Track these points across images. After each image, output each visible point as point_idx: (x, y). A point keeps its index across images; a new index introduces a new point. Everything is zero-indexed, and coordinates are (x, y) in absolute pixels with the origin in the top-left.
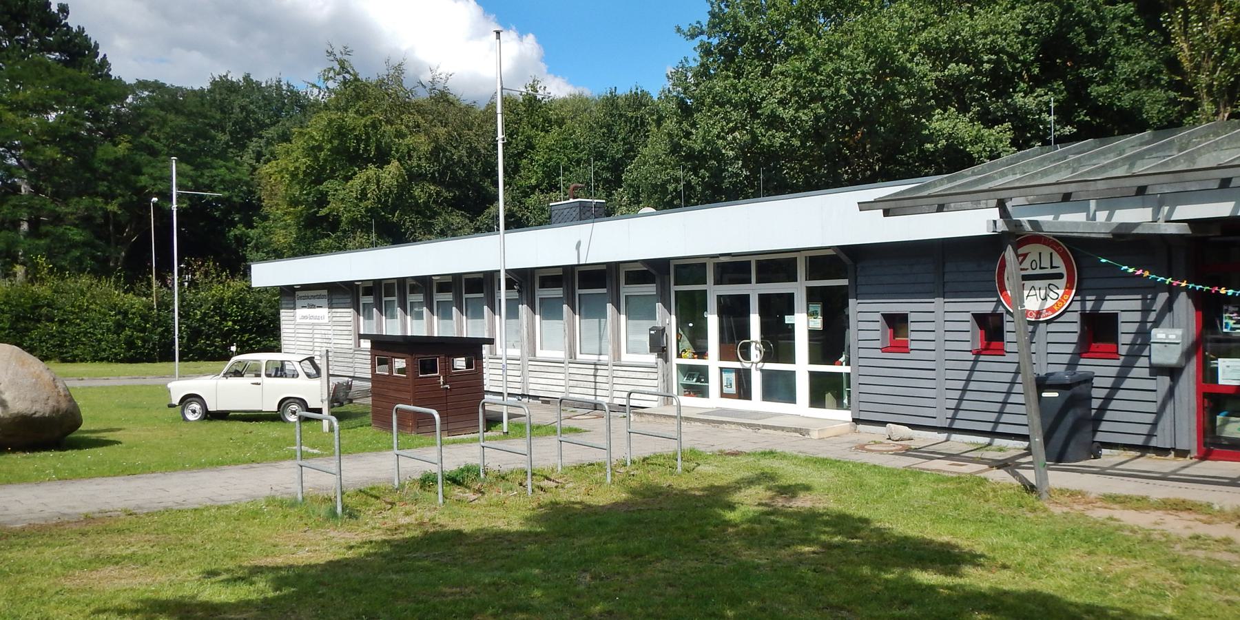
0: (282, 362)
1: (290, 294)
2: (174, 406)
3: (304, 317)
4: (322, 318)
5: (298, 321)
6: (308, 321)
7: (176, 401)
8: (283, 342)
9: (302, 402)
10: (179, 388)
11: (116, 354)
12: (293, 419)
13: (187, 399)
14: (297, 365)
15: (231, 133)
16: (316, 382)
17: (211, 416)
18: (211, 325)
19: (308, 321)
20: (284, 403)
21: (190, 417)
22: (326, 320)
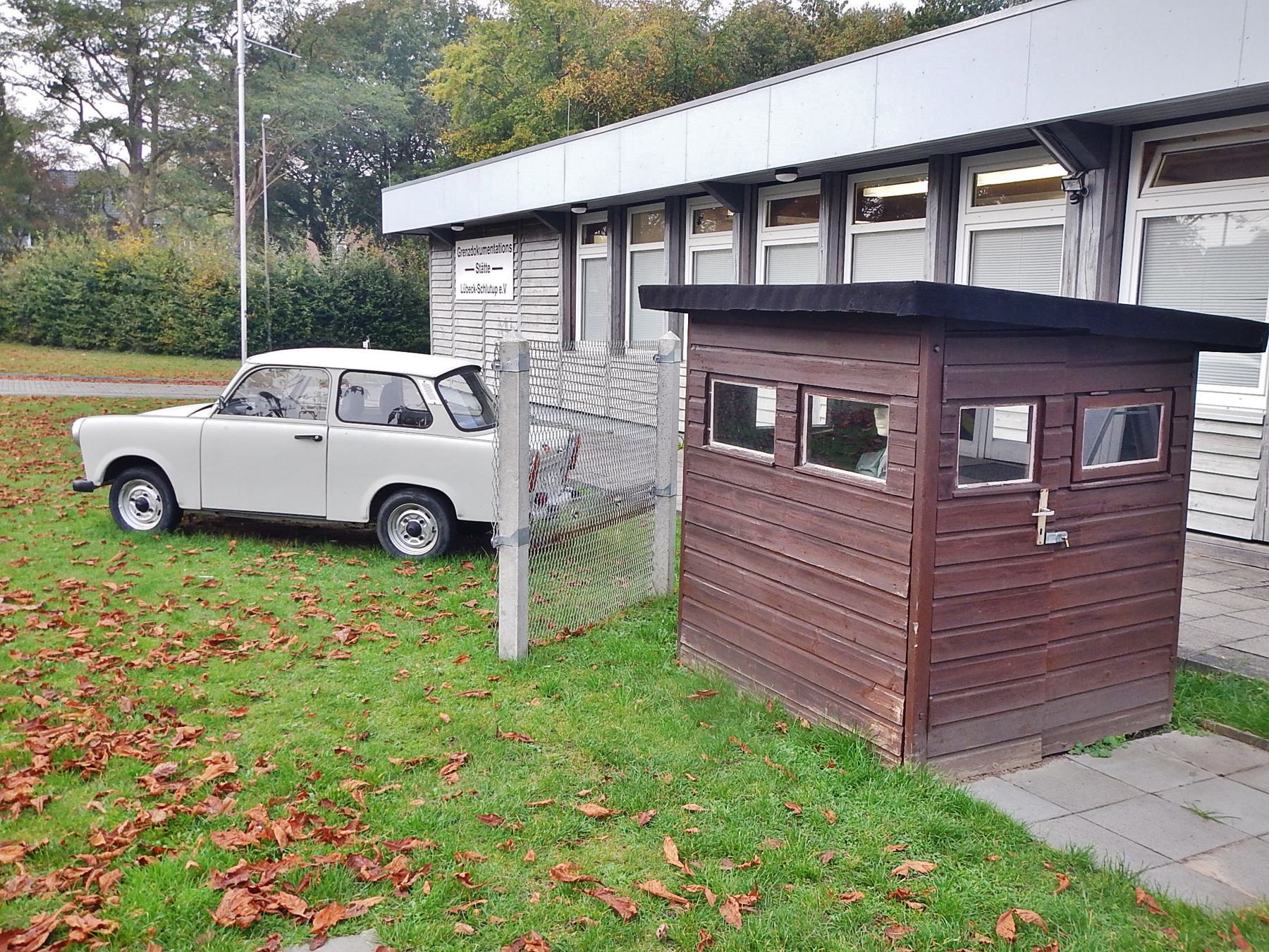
0: (525, 344)
1: (445, 238)
2: (89, 487)
3: (469, 290)
4: (502, 289)
5: (459, 296)
6: (476, 296)
7: (95, 473)
8: (433, 335)
9: (439, 502)
10: (102, 437)
11: (214, 345)
12: (409, 547)
13: (126, 470)
14: (428, 389)
15: (390, 52)
16: (485, 441)
17: (178, 522)
18: (342, 310)
19: (476, 296)
20: (389, 498)
21: (130, 516)
22: (509, 295)
